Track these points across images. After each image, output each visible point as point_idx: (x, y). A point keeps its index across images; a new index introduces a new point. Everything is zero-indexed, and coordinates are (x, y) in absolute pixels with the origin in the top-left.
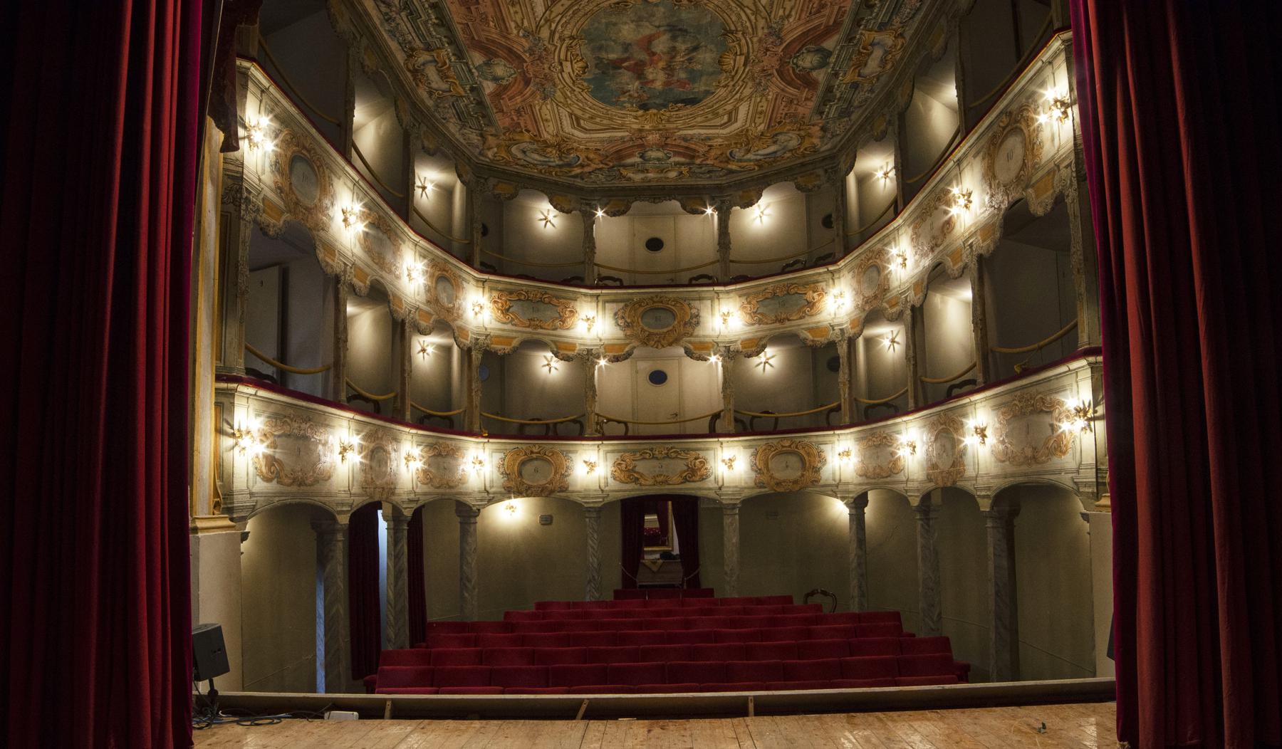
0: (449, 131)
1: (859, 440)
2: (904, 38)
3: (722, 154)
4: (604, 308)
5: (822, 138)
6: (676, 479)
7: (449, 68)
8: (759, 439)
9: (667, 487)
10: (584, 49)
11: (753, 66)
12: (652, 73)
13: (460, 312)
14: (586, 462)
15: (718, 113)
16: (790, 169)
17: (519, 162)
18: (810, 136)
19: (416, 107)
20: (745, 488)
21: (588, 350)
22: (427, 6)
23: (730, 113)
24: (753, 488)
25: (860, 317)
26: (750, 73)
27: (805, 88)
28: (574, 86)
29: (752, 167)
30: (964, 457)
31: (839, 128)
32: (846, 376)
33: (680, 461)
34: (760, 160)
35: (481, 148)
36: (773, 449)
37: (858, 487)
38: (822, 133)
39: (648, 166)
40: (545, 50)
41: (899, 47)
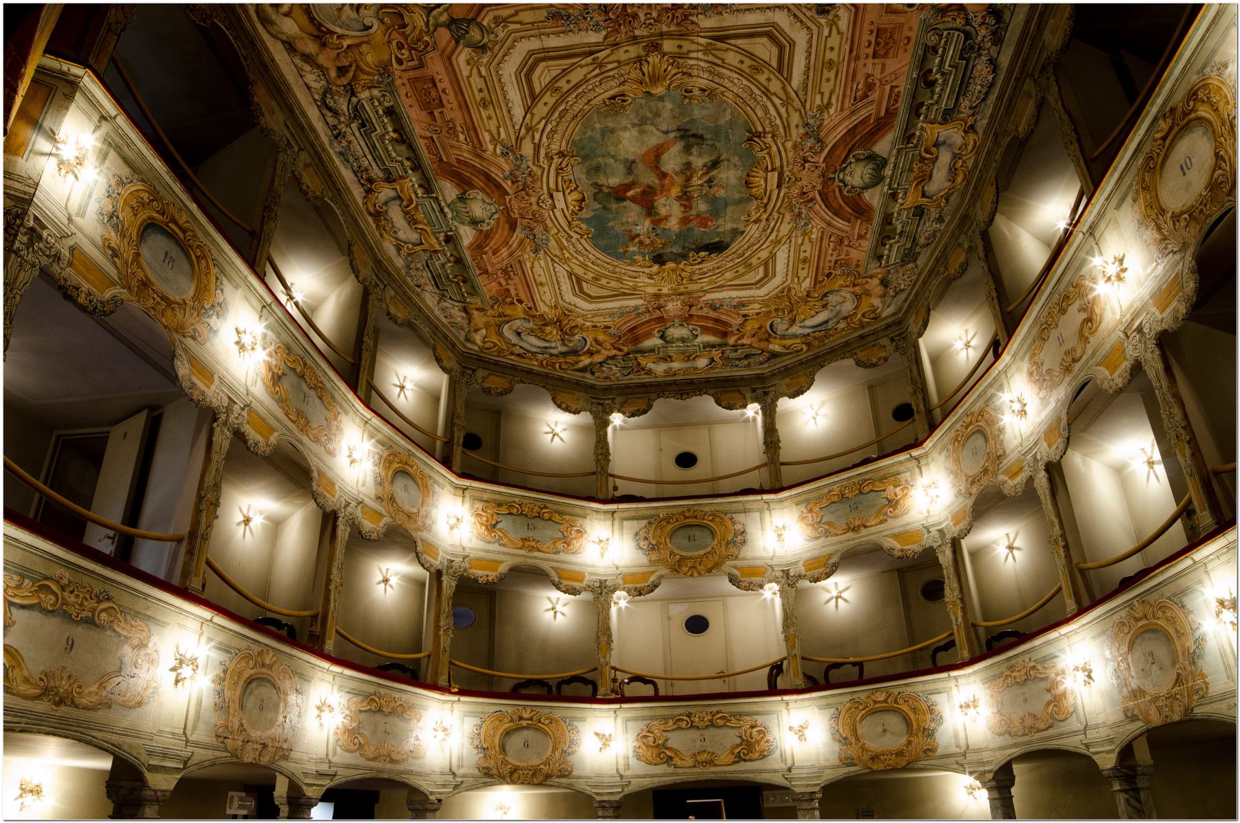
0: (427, 305)
1: (990, 680)
2: (975, 132)
3: (760, 328)
4: (621, 528)
6: (725, 757)
7: (416, 207)
8: (841, 694)
9: (713, 769)
10: (577, 172)
11: (788, 188)
13: (428, 522)
14: (597, 734)
15: (750, 265)
16: (847, 344)
17: (514, 349)
18: (868, 293)
20: (827, 767)
21: (601, 582)
22: (381, 112)
23: (766, 264)
24: (838, 767)
25: (966, 505)
26: (786, 200)
27: (857, 218)
28: (570, 229)
29: (799, 347)
30: (1200, 663)
31: (902, 279)
32: (956, 593)
33: (730, 731)
34: (808, 335)
36: (861, 707)
37: (998, 754)
39: (672, 350)
40: (530, 174)
41: (970, 148)
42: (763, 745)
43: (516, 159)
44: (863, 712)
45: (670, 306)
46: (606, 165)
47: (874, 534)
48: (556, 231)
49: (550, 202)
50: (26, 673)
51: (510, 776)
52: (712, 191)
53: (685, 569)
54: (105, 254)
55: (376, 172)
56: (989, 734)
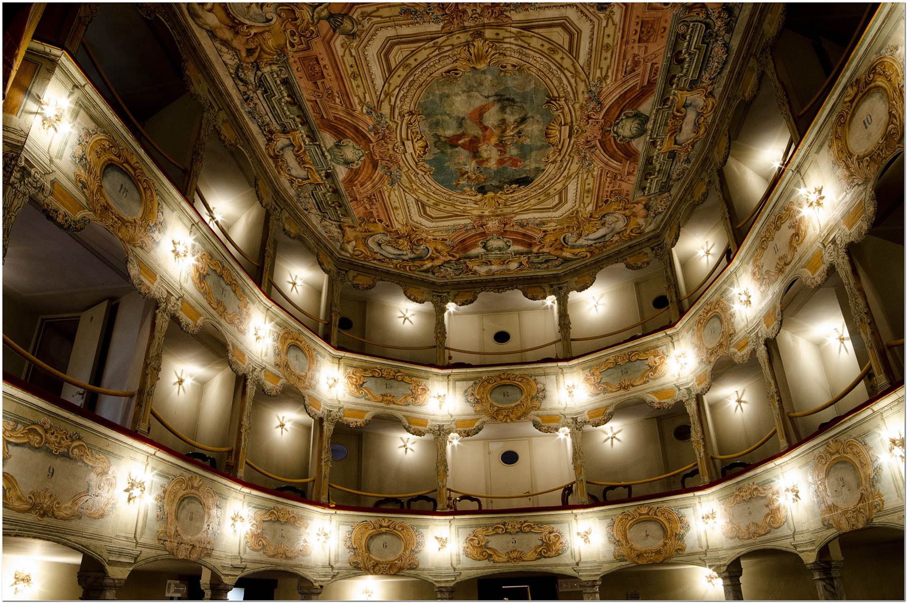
0: (312, 224)
1: (723, 499)
2: (713, 97)
3: (556, 240)
4: (454, 387)
5: (646, 217)
6: (531, 555)
7: (305, 151)
9: (521, 563)
10: (422, 126)
11: (577, 138)
13: (313, 382)
14: (437, 538)
16: (619, 252)
17: (376, 255)
18: (635, 215)
24: (613, 562)
25: (706, 370)
26: (575, 146)
27: (627, 160)
29: (584, 254)
30: (878, 485)
31: (660, 205)
32: (699, 434)
33: (534, 536)
34: (591, 245)
35: (341, 242)
36: (630, 518)
37: (730, 552)
39: (491, 256)
41: (709, 108)
42: (558, 546)
44: (631, 522)
45: (490, 224)
46: (443, 121)
49: (403, 148)
50: (19, 493)
51: (373, 569)
52: (521, 140)
53: (501, 417)
54: (77, 186)
55: (275, 126)
56: (724, 538)
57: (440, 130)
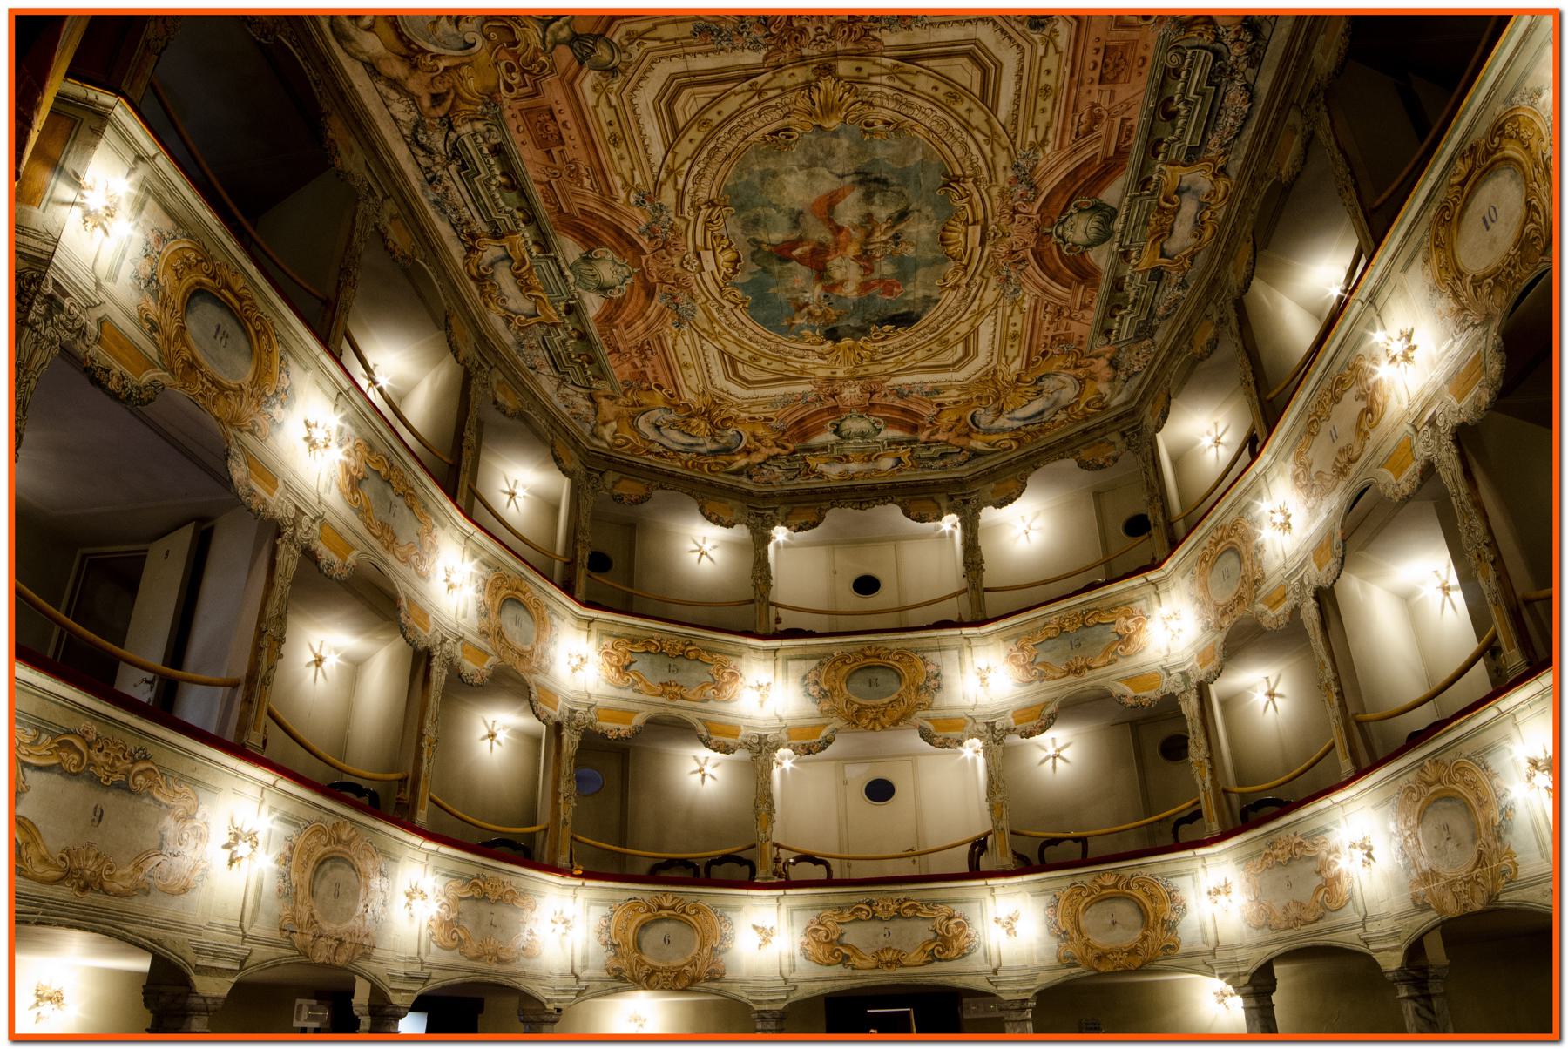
0: (543, 392)
1: (1245, 860)
2: (1227, 175)
3: (958, 420)
4: (786, 670)
5: (1113, 380)
6: (915, 956)
7: (530, 269)
10: (731, 226)
11: (994, 245)
12: (840, 267)
13: (545, 662)
14: (755, 927)
15: (947, 341)
16: (1067, 440)
18: (1093, 377)
19: (484, 341)
20: (1041, 969)
21: (760, 737)
22: (486, 151)
24: (1056, 968)
25: (1215, 642)
26: (991, 260)
30: (1507, 838)
31: (1135, 360)
32: (1203, 751)
33: (921, 923)
34: (1019, 429)
36: (1084, 894)
37: (1255, 952)
38: (1111, 371)
39: (849, 448)
41: (1220, 195)
43: (655, 209)
44: (1087, 900)
45: (846, 393)
46: (766, 217)
47: (1100, 677)
48: (704, 299)
49: (697, 263)
50: (43, 851)
51: (647, 980)
52: (899, 249)
53: (865, 721)
54: (141, 328)
55: (480, 226)
56: (1245, 928)
57: (761, 232)
